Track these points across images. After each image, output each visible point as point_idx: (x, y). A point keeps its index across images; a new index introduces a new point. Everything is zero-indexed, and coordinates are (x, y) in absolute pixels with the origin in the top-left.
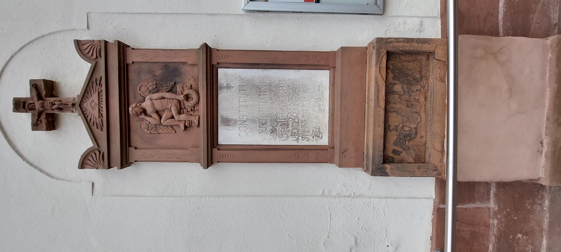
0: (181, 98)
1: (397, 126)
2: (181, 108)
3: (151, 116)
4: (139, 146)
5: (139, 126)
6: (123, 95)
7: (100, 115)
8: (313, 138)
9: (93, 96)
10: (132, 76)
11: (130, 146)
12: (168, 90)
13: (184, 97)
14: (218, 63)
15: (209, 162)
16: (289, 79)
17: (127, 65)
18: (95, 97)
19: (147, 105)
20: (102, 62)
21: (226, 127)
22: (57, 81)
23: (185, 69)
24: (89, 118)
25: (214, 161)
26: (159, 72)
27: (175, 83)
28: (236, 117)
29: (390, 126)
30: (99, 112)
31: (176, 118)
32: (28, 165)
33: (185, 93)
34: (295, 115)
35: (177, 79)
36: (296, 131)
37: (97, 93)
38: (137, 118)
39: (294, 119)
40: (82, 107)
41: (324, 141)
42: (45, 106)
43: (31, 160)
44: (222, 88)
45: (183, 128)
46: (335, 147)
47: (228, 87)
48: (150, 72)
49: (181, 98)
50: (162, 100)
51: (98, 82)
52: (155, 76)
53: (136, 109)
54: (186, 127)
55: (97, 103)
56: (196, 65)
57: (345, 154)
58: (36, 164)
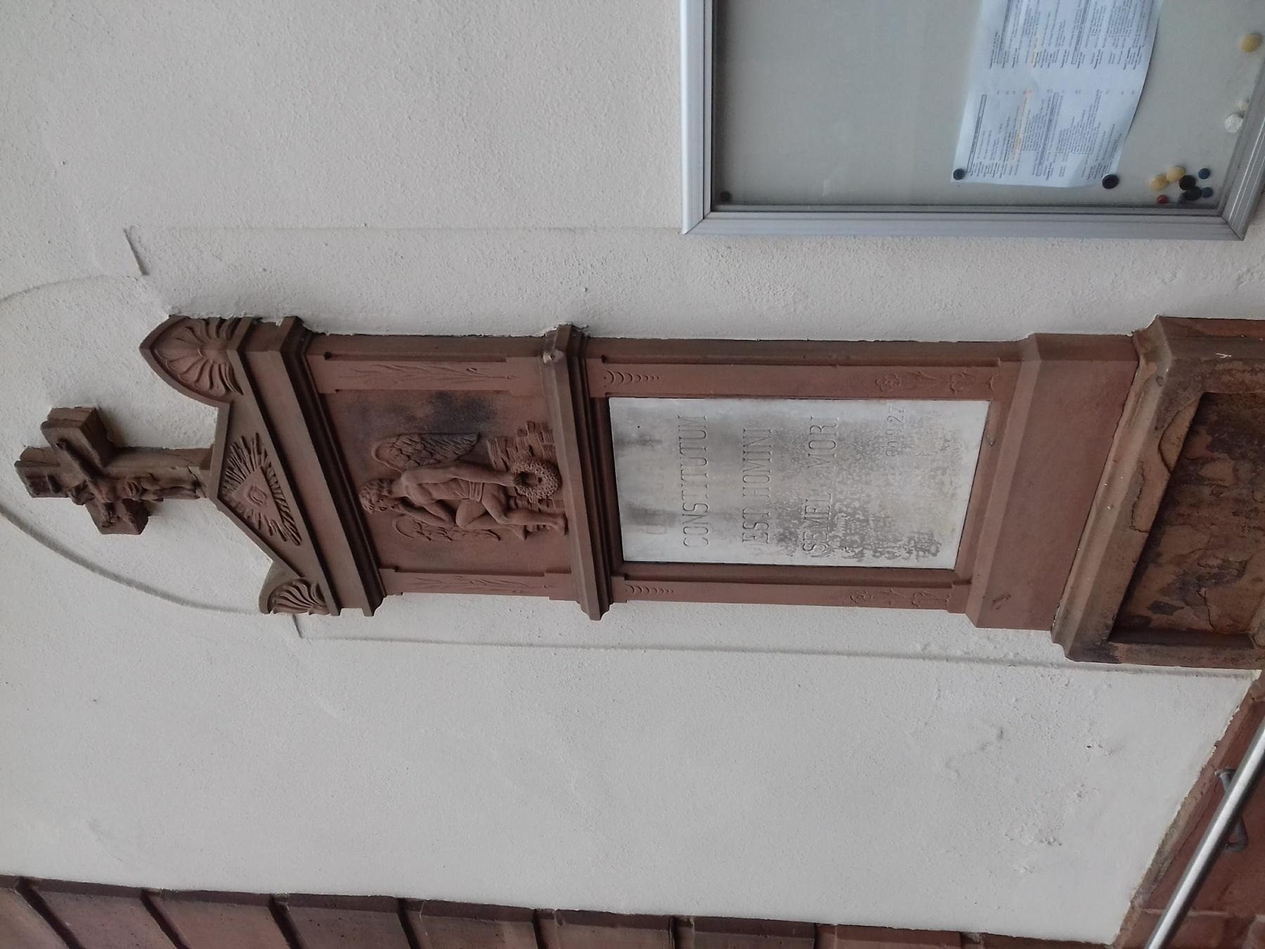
0: (509, 481)
1: (1184, 556)
4: (404, 562)
6: (333, 472)
7: (284, 515)
8: (910, 552)
11: (380, 565)
15: (602, 601)
16: (845, 424)
17: (323, 397)
20: (248, 401)
21: (645, 527)
22: (104, 405)
24: (255, 521)
25: (615, 595)
27: (480, 437)
28: (676, 507)
29: (1159, 555)
30: (279, 509)
32: (124, 587)
33: (518, 467)
34: (857, 504)
36: (856, 538)
37: (258, 470)
39: (853, 515)
41: (946, 558)
44: (624, 443)
45: (521, 537)
46: (974, 581)
47: (644, 441)
51: (253, 447)
52: (411, 418)
55: (268, 492)
57: (998, 604)
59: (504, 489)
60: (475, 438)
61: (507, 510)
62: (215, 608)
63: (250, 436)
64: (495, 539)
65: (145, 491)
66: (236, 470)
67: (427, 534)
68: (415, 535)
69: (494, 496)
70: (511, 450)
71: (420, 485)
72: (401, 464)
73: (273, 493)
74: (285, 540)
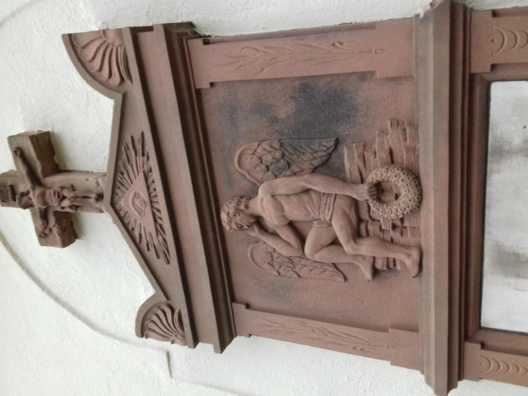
0: (362, 193)
2: (360, 220)
3: (274, 234)
4: (254, 301)
5: (249, 255)
9: (135, 181)
10: (216, 123)
11: (233, 299)
12: (316, 163)
13: (370, 191)
14: (493, 67)
17: (199, 92)
18: (138, 185)
19: (262, 205)
21: (513, 281)
22: (56, 130)
23: (364, 94)
24: (136, 233)
26: (285, 110)
27: (337, 142)
30: (155, 221)
31: (348, 248)
33: (372, 177)
35: (342, 129)
38: (241, 235)
40: (117, 206)
42: (49, 201)
43: (54, 290)
45: (368, 275)
48: (262, 108)
49: (362, 193)
50: (305, 197)
51: (139, 147)
52: (274, 120)
53: (238, 219)
54: (375, 272)
55: (147, 199)
56: (409, 78)
58: (63, 297)
59: (355, 204)
60: (331, 143)
61: (357, 235)
62: (115, 337)
63: (138, 138)
64: (341, 279)
65: (64, 198)
66: (126, 175)
67: (277, 267)
68: (267, 266)
69: (345, 215)
70: (369, 156)
71: (273, 196)
72: (259, 176)
73: (151, 202)
74: (158, 257)
